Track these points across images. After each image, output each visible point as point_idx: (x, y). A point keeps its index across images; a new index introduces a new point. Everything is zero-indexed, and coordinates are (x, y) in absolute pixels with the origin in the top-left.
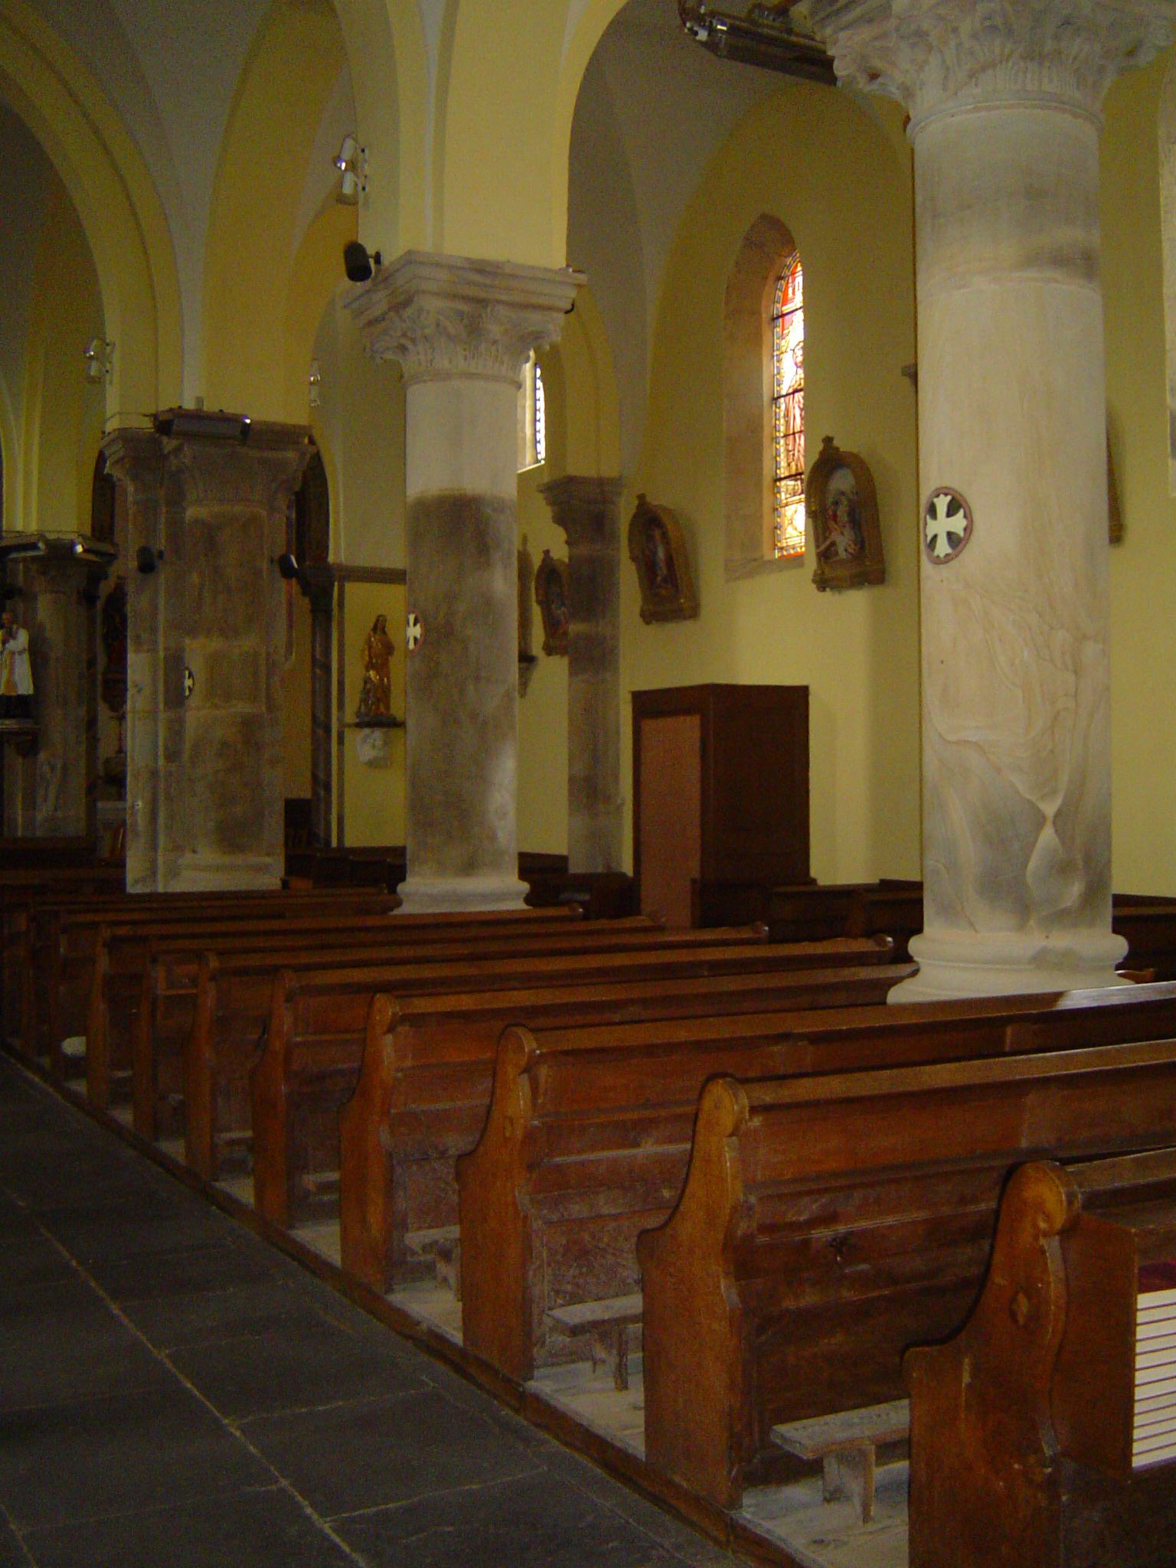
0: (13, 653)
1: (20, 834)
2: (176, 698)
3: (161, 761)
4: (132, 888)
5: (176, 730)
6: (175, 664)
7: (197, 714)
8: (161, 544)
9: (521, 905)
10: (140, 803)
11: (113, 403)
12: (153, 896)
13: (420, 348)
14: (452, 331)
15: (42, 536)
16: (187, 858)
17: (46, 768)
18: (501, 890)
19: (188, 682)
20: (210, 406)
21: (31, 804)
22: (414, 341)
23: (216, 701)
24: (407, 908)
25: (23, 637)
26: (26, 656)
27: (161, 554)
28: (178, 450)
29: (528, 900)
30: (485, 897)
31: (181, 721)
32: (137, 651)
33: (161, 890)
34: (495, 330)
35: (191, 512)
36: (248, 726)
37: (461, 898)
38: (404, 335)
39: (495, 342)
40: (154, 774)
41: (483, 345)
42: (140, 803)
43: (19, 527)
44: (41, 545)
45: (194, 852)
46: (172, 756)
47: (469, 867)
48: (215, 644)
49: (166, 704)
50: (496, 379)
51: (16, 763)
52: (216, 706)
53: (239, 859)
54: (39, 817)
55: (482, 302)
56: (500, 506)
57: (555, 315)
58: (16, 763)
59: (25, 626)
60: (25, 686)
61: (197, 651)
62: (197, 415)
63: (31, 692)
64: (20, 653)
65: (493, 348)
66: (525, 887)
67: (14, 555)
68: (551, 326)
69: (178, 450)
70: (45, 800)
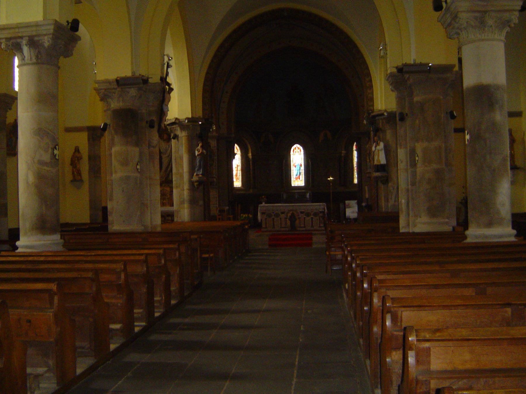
0: (378, 151)
1: (384, 210)
2: (413, 164)
3: (410, 186)
4: (402, 231)
5: (414, 174)
6: (412, 153)
7: (420, 169)
8: (406, 111)
9: (513, 239)
10: (403, 201)
11: (112, 106)
12: (408, 233)
13: (463, 32)
14: (473, 24)
15: (386, 111)
16: (419, 220)
17: (391, 188)
18: (504, 232)
19: (417, 158)
20: (418, 61)
21: (387, 200)
22: (461, 29)
23: (426, 164)
24: (469, 240)
25: (382, 145)
26: (383, 151)
27: (407, 115)
28: (409, 78)
29: (516, 236)
30: (495, 236)
31: (416, 172)
32: (401, 148)
33: (411, 231)
34: (490, 22)
35: (416, 99)
36: (438, 173)
37: (486, 237)
38: (458, 28)
39: (491, 26)
40: (408, 190)
41: (486, 29)
42: (403, 201)
43: (380, 108)
44: (386, 114)
45: (420, 217)
46: (413, 184)
47: (490, 224)
48: (425, 144)
49: (410, 165)
50: (493, 40)
51: (382, 187)
52: (426, 166)
53: (435, 220)
54: (390, 205)
55: (485, 12)
56: (498, 87)
57: (514, 12)
58: (382, 187)
59: (383, 141)
60: (383, 161)
61: (419, 147)
62: (415, 65)
63: (385, 163)
64: (382, 150)
65: (491, 29)
66: (514, 232)
67: (377, 118)
68: (513, 17)
69: (409, 78)
70: (391, 199)
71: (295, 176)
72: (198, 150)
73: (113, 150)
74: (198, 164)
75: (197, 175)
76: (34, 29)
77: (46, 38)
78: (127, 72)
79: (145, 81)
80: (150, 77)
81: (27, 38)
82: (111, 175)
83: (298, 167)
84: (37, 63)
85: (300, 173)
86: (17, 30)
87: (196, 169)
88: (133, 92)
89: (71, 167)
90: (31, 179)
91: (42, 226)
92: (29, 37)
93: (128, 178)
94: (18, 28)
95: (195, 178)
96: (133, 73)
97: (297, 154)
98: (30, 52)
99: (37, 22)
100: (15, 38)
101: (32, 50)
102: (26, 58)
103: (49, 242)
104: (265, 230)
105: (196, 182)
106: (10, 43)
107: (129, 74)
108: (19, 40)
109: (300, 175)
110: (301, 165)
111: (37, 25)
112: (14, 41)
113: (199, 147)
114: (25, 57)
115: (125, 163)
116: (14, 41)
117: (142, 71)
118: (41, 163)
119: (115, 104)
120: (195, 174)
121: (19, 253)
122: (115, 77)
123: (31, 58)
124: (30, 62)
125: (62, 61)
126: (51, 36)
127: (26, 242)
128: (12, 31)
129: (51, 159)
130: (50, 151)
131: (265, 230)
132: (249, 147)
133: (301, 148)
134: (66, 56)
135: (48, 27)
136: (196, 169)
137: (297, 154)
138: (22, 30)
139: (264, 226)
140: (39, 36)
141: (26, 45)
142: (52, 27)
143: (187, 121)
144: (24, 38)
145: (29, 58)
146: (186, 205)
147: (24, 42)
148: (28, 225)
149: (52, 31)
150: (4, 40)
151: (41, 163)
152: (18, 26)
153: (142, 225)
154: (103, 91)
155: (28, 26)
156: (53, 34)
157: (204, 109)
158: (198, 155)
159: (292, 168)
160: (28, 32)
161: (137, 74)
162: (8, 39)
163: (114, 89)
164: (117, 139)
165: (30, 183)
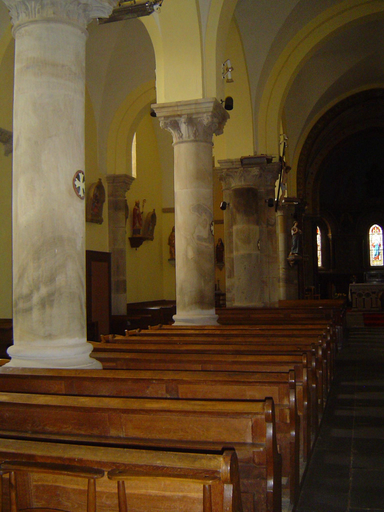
71: (374, 256)
72: (293, 230)
73: (235, 228)
74: (294, 243)
75: (293, 254)
76: (193, 107)
77: (205, 115)
78: (249, 152)
79: (269, 160)
80: (273, 156)
81: (186, 116)
82: (232, 252)
83: (377, 248)
84: (195, 141)
85: (379, 253)
86: (176, 109)
87: (292, 248)
88: (255, 171)
89: (169, 247)
90: (191, 254)
91: (201, 301)
92: (188, 115)
93: (250, 255)
94: (177, 106)
95: (291, 257)
96: (255, 152)
97: (376, 234)
98: (188, 129)
99: (197, 100)
100: (174, 116)
101: (190, 128)
102: (184, 136)
103: (207, 316)
104: (356, 309)
105: (292, 261)
106: (168, 121)
107: (252, 154)
108: (177, 119)
109: (379, 255)
110: (380, 245)
111: (197, 103)
112: (173, 119)
113: (295, 227)
114: (182, 135)
115: (247, 241)
116: (173, 119)
117: (261, 151)
118: (200, 238)
119: (236, 183)
120: (291, 253)
121: (177, 326)
122: (240, 157)
123: (189, 136)
124: (189, 140)
125: (215, 138)
126: (210, 114)
127: (183, 316)
128: (171, 109)
129: (209, 235)
130: (208, 226)
131: (356, 309)
132: (329, 227)
133: (380, 228)
134: (218, 134)
135: (207, 105)
136: (292, 248)
137: (376, 234)
138: (180, 108)
139: (354, 306)
140: (197, 113)
141: (185, 123)
142: (212, 105)
143: (283, 201)
144: (183, 116)
145: (187, 136)
146: (281, 284)
147: (183, 120)
148: (186, 299)
149: (211, 109)
150: (163, 119)
151: (200, 238)
152: (178, 105)
153: (263, 303)
154: (226, 170)
155: (188, 104)
156: (212, 112)
157: (298, 190)
158: (294, 234)
159: (371, 248)
160: (186, 110)
161: (259, 154)
162: (166, 117)
163: (237, 168)
164: (239, 217)
165: (190, 258)
